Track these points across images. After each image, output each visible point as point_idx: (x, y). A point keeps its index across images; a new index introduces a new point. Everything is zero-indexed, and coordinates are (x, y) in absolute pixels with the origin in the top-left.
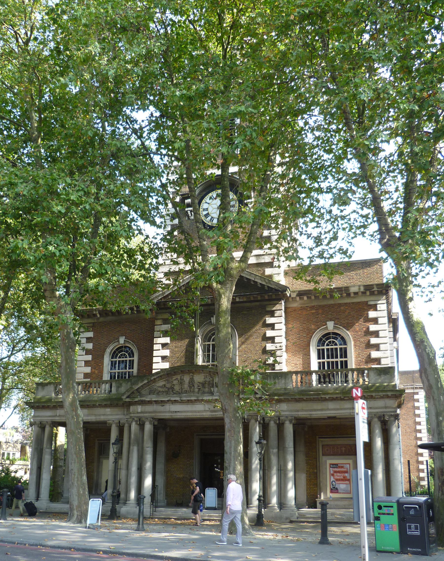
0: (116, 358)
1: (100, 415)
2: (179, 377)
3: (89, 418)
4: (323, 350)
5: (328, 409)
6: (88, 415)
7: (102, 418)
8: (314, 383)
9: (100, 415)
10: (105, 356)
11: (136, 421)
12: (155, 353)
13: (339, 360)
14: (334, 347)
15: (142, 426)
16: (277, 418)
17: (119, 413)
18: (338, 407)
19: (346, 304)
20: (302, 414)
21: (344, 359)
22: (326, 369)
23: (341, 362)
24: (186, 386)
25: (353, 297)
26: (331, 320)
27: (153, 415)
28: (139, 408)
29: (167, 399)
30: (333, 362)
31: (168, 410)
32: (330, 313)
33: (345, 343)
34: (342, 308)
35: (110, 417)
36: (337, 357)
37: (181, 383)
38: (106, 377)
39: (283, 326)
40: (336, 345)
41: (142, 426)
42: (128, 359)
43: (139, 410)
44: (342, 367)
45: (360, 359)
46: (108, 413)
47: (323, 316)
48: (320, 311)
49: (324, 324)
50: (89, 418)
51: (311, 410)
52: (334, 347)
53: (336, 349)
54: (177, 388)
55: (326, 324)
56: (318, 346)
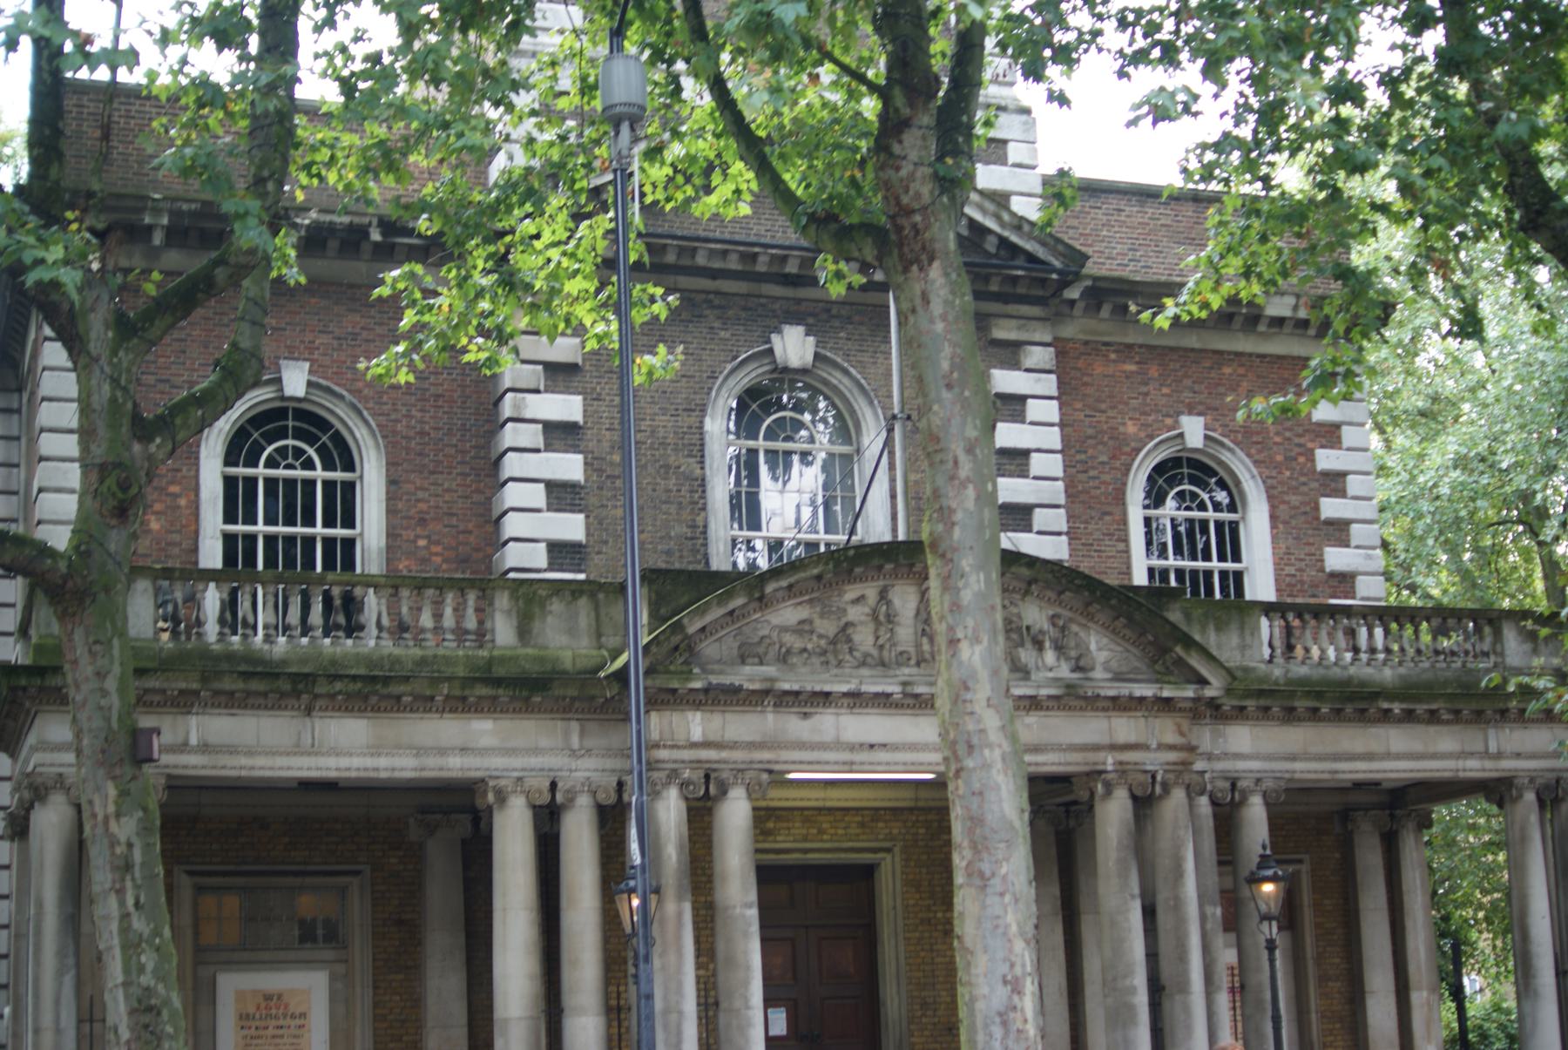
0: (256, 465)
1: (442, 751)
2: (871, 591)
3: (383, 762)
4: (251, 482)
5: (1388, 756)
6: (375, 750)
7: (455, 766)
8: (212, 629)
9: (442, 751)
10: (204, 452)
11: (684, 785)
12: (513, 465)
13: (1215, 564)
14: (299, 473)
15: (701, 814)
16: (1227, 785)
17: (544, 742)
18: (1418, 747)
19: (1239, 354)
20: (1305, 770)
21: (339, 532)
22: (1218, 595)
23: (329, 543)
24: (905, 633)
25: (1261, 334)
26: (1191, 410)
27: (766, 755)
28: (696, 724)
29: (844, 688)
30: (290, 540)
31: (828, 736)
32: (1188, 382)
33: (349, 466)
34: (1227, 370)
35: (497, 762)
36: (309, 521)
37: (884, 618)
38: (211, 555)
39: (1048, 410)
40: (309, 465)
41: (701, 814)
42: (319, 474)
43: (697, 734)
44: (329, 563)
45: (1292, 570)
46: (486, 741)
47: (1165, 390)
48: (1154, 371)
49: (1169, 421)
50: (383, 762)
51: (1337, 757)
52: (299, 473)
53: (309, 484)
54: (864, 638)
55: (1176, 425)
56: (1146, 507)
